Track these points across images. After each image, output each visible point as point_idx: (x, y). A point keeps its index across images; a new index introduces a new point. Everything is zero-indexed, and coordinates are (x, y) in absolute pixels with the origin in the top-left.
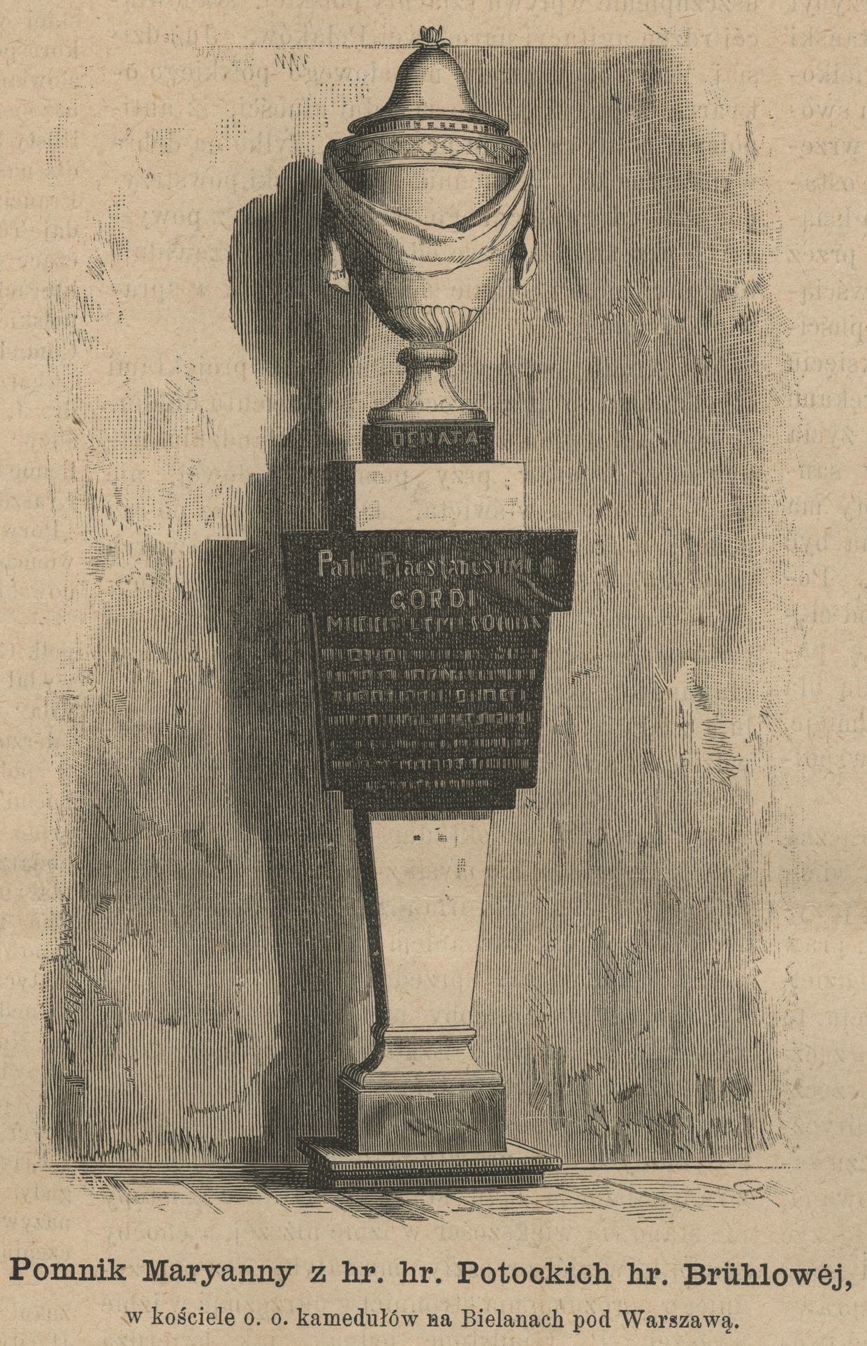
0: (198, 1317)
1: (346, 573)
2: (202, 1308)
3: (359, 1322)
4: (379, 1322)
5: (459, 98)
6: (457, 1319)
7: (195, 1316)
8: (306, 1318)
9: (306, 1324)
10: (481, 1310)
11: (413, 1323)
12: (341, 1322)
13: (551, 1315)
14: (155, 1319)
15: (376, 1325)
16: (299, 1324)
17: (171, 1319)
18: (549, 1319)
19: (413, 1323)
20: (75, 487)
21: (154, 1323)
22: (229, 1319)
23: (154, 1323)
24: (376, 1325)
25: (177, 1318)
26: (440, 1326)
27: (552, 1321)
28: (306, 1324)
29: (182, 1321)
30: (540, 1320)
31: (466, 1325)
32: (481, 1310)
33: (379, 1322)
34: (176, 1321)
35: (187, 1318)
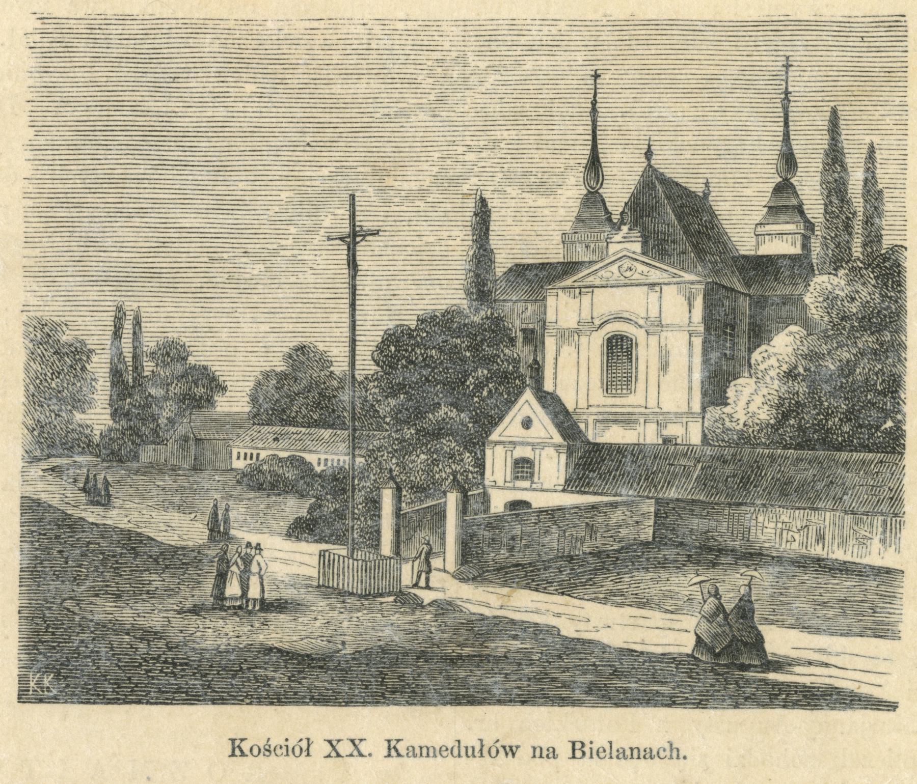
0: (284, 748)
1: (341, 586)
2: (287, 740)
3: (456, 752)
4: (477, 754)
5: (476, 591)
6: (564, 750)
7: (281, 747)
8: (398, 746)
9: (243, 754)
10: (591, 743)
11: (514, 754)
12: (437, 753)
13: (667, 746)
14: (389, 749)
15: (474, 757)
16: (233, 755)
17: (413, 752)
18: (664, 750)
19: (514, 754)
20: (619, 627)
21: (233, 755)
22: (511, 751)
23: (233, 755)
24: (474, 757)
25: (262, 750)
26: (464, 757)
27: (668, 753)
28: (243, 754)
29: (267, 753)
30: (655, 753)
31: (574, 757)
32: (591, 743)
33: (477, 754)
34: (262, 754)
35: (272, 749)
